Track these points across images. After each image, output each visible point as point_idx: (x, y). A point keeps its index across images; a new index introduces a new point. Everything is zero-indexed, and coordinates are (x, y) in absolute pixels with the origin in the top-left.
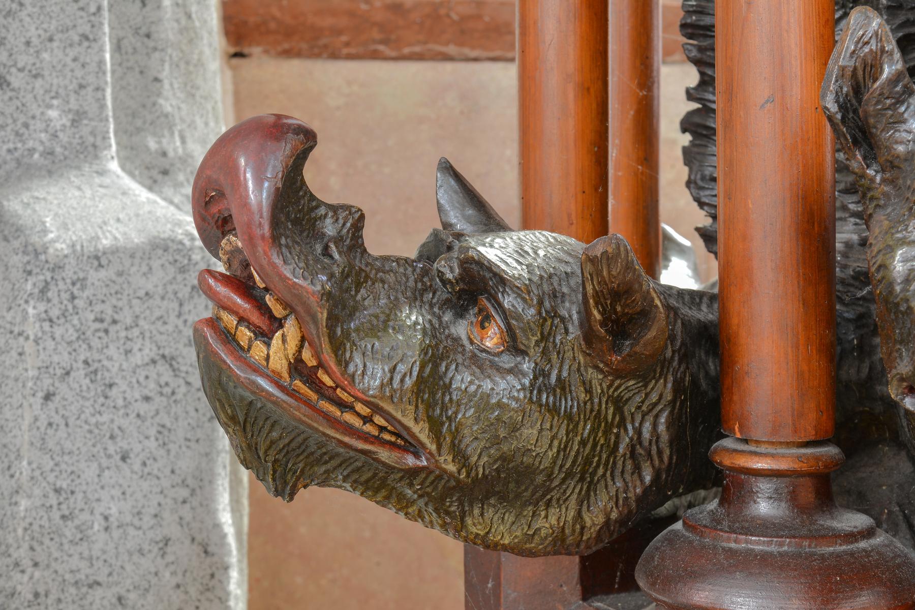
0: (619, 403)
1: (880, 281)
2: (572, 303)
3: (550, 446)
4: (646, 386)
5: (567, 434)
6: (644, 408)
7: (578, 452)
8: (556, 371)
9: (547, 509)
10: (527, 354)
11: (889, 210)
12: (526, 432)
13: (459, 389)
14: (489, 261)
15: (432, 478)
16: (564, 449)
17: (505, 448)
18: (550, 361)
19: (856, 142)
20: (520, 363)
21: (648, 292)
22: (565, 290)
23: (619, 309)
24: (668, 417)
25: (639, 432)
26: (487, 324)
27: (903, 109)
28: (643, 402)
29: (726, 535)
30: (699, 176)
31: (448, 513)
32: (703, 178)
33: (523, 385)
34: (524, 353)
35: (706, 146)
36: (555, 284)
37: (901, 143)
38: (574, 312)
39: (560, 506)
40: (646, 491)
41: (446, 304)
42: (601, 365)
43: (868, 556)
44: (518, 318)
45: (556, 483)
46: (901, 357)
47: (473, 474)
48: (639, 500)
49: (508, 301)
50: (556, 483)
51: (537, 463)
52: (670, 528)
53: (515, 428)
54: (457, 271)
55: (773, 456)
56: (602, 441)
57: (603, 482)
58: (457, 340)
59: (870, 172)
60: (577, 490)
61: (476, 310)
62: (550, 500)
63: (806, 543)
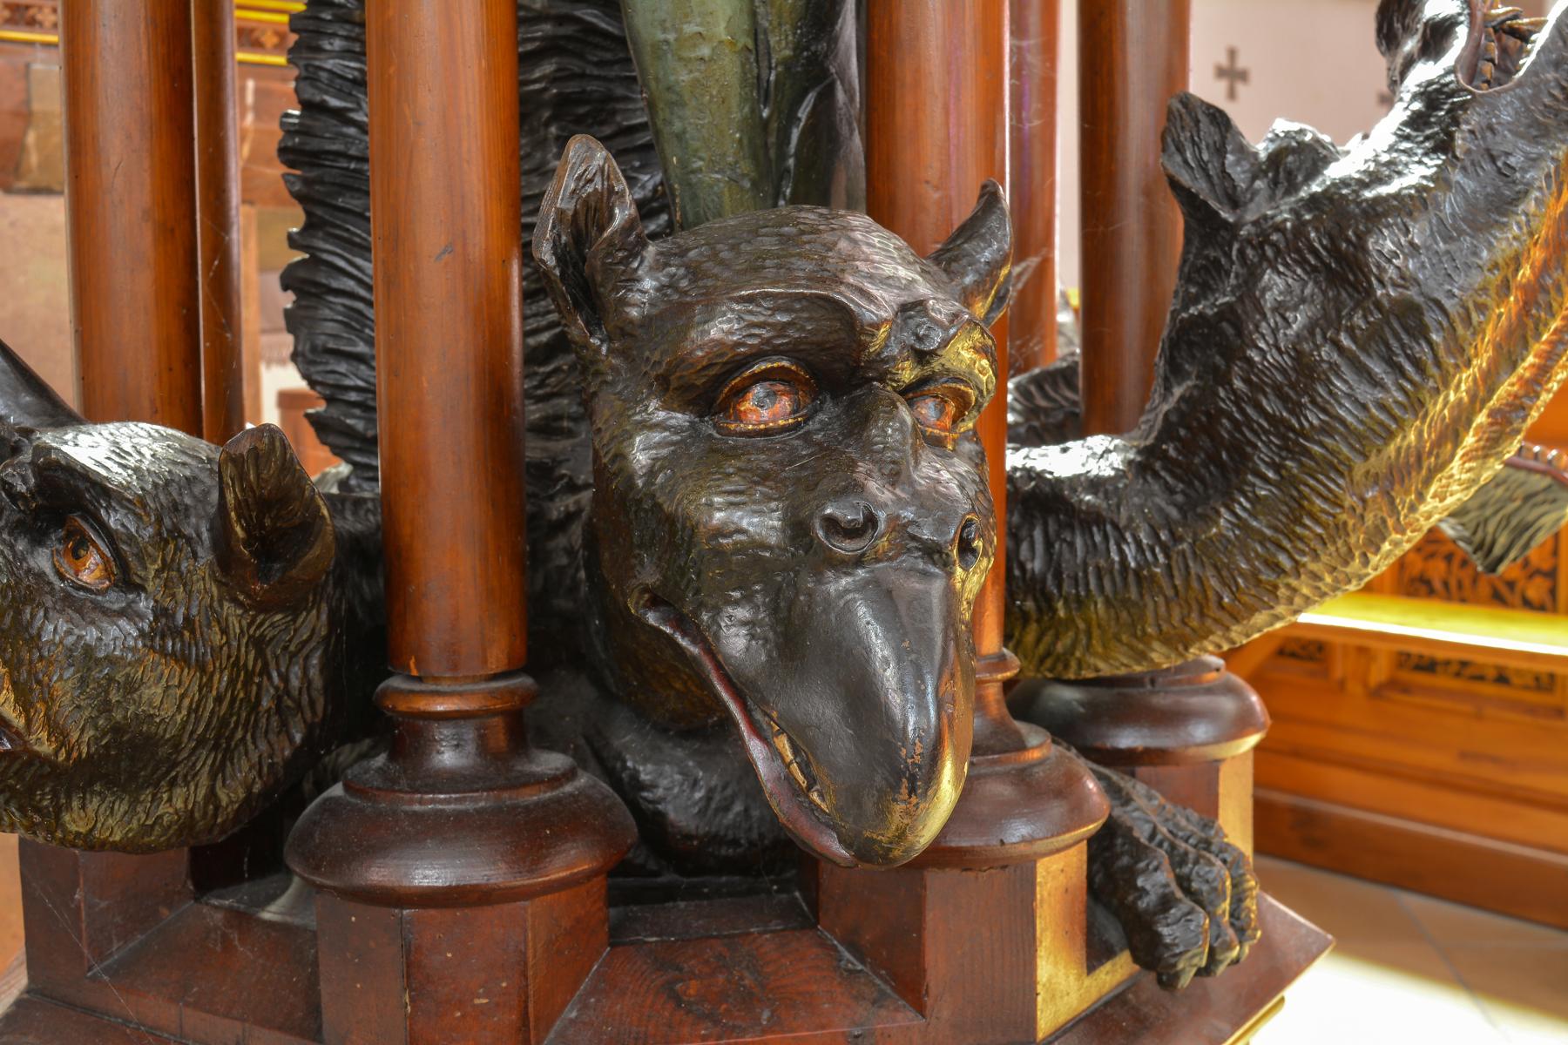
0: (259, 644)
1: (616, 475)
2: (199, 517)
3: (179, 708)
4: (294, 621)
5: (200, 690)
6: (292, 648)
7: (212, 712)
8: (183, 610)
9: (170, 790)
10: (144, 589)
11: (620, 387)
12: (146, 693)
13: (52, 642)
14: (83, 466)
15: (16, 766)
16: (194, 710)
17: (118, 715)
18: (173, 596)
19: (577, 306)
20: (133, 601)
21: (312, 498)
22: (188, 500)
23: (267, 522)
24: (321, 657)
25: (285, 678)
26: (82, 552)
27: (635, 265)
28: (290, 641)
29: (407, 797)
30: (308, 347)
31: (38, 810)
32: (314, 349)
33: (141, 631)
34: (140, 589)
35: (316, 308)
36: (175, 494)
37: (634, 305)
38: (204, 530)
39: (187, 784)
40: (297, 752)
41: (18, 528)
42: (241, 598)
43: (576, 801)
44: (131, 539)
45: (184, 754)
46: (642, 564)
47: (75, 754)
48: (288, 763)
49: (114, 519)
50: (184, 754)
51: (161, 731)
52: (325, 795)
53: (130, 687)
54: (33, 481)
55: (460, 694)
56: (242, 695)
57: (241, 748)
58: (40, 575)
59: (595, 341)
60: (209, 762)
61: (62, 533)
62: (175, 778)
63: (506, 795)
